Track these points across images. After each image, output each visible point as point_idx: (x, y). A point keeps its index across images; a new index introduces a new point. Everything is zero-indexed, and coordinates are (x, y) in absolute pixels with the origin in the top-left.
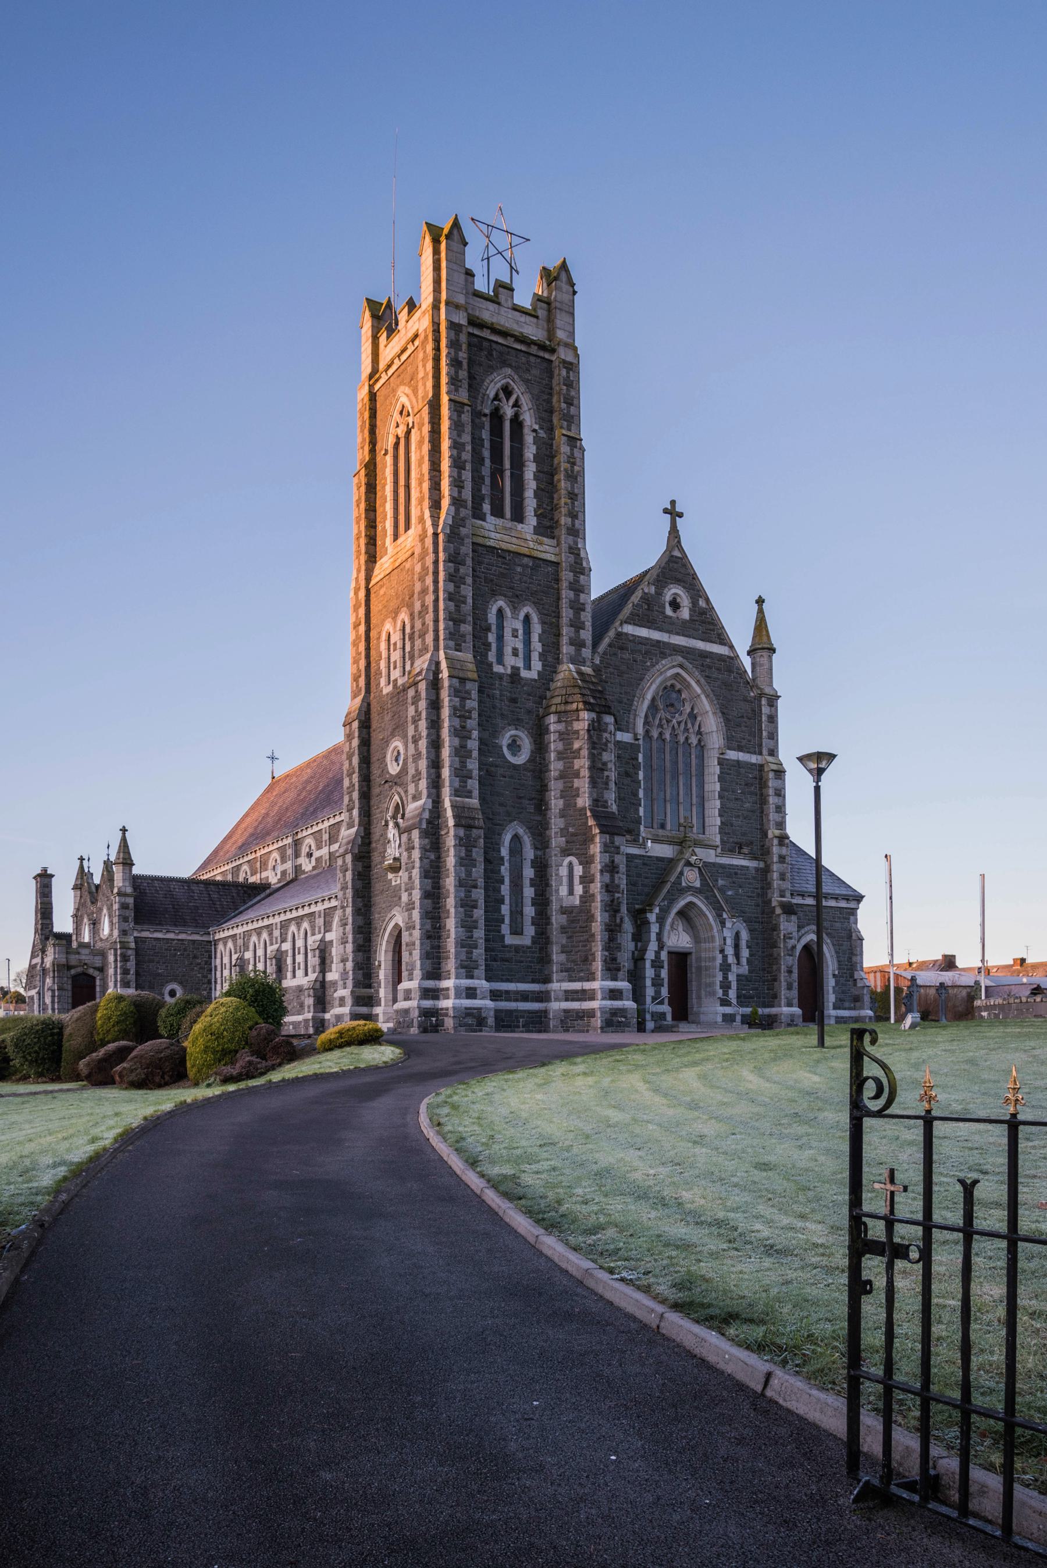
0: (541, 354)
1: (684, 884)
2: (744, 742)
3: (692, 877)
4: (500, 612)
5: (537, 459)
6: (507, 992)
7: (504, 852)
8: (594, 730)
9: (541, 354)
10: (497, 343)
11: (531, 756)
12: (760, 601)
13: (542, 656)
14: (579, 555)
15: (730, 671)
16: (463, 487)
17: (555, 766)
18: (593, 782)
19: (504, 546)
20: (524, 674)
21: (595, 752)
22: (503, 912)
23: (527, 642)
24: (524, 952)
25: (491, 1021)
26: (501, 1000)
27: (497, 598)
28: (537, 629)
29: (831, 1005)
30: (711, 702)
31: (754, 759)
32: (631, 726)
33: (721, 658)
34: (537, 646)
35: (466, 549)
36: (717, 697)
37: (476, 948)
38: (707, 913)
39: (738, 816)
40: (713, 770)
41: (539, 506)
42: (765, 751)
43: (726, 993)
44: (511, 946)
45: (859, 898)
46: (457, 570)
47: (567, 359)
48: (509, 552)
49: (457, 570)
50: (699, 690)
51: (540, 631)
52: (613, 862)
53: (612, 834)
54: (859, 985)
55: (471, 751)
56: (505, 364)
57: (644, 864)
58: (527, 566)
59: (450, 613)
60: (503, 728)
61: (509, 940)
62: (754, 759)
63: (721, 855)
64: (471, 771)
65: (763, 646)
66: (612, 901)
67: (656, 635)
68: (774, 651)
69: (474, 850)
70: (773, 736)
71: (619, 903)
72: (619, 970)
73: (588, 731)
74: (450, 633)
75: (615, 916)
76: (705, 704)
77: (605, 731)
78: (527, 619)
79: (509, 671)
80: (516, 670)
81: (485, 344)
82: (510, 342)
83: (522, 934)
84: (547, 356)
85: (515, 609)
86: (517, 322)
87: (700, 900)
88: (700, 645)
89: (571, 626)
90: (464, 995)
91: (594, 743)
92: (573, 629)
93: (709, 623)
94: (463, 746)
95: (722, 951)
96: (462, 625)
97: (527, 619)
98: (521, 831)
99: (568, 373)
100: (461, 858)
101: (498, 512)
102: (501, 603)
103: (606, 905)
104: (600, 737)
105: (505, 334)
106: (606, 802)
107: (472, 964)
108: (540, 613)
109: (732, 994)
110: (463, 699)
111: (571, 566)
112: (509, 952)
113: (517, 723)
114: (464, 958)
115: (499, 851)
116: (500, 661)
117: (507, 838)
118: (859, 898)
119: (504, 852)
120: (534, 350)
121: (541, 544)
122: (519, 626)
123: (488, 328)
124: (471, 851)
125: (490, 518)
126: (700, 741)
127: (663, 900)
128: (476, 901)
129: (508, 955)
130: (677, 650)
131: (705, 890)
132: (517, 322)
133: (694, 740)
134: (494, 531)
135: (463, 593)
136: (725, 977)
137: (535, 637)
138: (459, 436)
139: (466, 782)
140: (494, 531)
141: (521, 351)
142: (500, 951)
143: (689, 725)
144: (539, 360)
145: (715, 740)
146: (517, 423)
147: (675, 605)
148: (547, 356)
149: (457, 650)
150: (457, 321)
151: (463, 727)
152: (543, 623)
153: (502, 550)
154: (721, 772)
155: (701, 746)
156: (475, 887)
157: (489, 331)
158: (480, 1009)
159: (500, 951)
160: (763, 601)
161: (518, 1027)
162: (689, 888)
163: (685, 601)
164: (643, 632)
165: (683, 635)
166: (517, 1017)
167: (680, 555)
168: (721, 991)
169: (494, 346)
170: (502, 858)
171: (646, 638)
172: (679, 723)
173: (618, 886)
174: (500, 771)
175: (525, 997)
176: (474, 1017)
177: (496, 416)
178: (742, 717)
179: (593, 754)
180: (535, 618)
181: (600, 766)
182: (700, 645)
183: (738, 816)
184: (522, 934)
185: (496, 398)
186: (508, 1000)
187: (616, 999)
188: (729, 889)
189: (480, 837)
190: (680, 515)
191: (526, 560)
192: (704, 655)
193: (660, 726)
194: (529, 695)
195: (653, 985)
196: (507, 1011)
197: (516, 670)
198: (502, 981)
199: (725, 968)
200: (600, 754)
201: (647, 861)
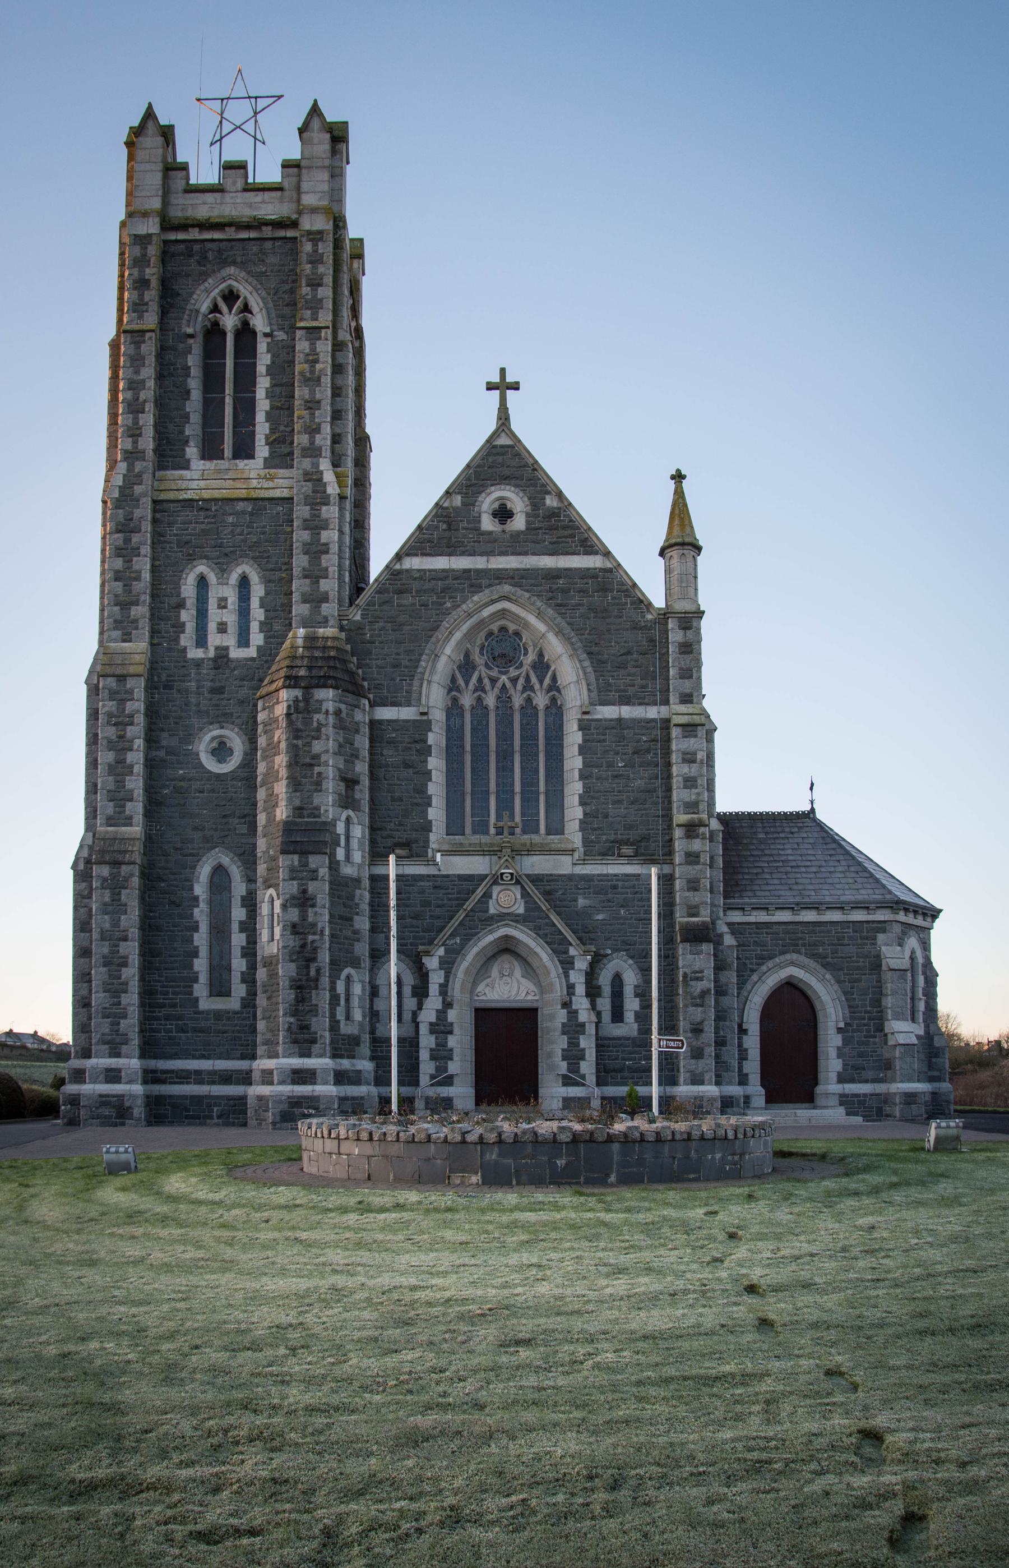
0: (282, 233)
1: (492, 911)
2: (631, 691)
3: (507, 899)
4: (202, 582)
5: (270, 371)
6: (198, 1072)
7: (200, 890)
8: (297, 711)
9: (282, 233)
10: (213, 240)
11: (244, 759)
12: (678, 477)
13: (265, 626)
14: (320, 480)
15: (604, 589)
16: (140, 435)
17: (427, 1041)
18: (295, 784)
19: (206, 494)
20: (236, 653)
21: (300, 742)
22: (196, 968)
23: (244, 613)
24: (229, 1019)
25: (139, 1111)
26: (188, 1083)
27: (195, 563)
28: (258, 591)
29: (833, 1076)
30: (566, 639)
31: (652, 712)
32: (414, 696)
33: (586, 574)
34: (257, 613)
35: (144, 511)
36: (579, 631)
37: (125, 1017)
38: (538, 950)
39: (619, 802)
40: (573, 737)
41: (273, 430)
42: (673, 698)
43: (573, 1067)
44: (208, 1012)
45: (932, 913)
46: (127, 541)
47: (315, 228)
48: (216, 500)
49: (127, 541)
50: (542, 627)
51: (262, 593)
52: (305, 891)
53: (304, 853)
54: (891, 1043)
55: (132, 766)
56: (225, 263)
57: (435, 887)
58: (244, 512)
59: (116, 596)
60: (201, 729)
61: (207, 1003)
62: (652, 712)
63: (583, 861)
64: (132, 791)
65: (681, 544)
66: (303, 946)
67: (479, 563)
68: (698, 549)
69: (123, 892)
70: (692, 671)
71: (315, 949)
72: (314, 1041)
73: (288, 715)
74: (115, 621)
75: (308, 967)
76: (555, 647)
77: (318, 711)
78: (244, 582)
79: (211, 654)
80: (222, 652)
81: (196, 247)
82: (231, 233)
83: (229, 995)
84: (290, 233)
85: (223, 571)
86: (250, 205)
87: (523, 932)
88: (548, 562)
89: (305, 577)
90: (102, 1077)
91: (298, 730)
92: (308, 581)
93: (565, 528)
94: (120, 761)
95: (566, 1005)
96: (133, 608)
97: (244, 582)
98: (226, 860)
99: (315, 246)
100: (105, 904)
101: (211, 451)
102: (202, 568)
103: (291, 954)
104: (308, 721)
105: (219, 226)
106: (318, 808)
107: (118, 1039)
108: (263, 569)
109: (588, 1067)
110: (122, 702)
111: (307, 497)
112: (206, 1019)
113: (222, 718)
114: (107, 1031)
115: (192, 889)
116: (201, 641)
117: (204, 871)
118: (932, 913)
119: (200, 890)
120: (267, 232)
121: (272, 479)
122: (231, 595)
123: (193, 226)
124: (119, 893)
125: (198, 465)
126: (554, 700)
127: (452, 935)
128: (127, 957)
129: (203, 1024)
130: (500, 576)
131: (532, 918)
132: (250, 205)
133: (541, 700)
134: (199, 478)
135: (136, 567)
136: (573, 1043)
137: (255, 603)
138: (137, 372)
139: (124, 806)
140: (199, 478)
141: (249, 239)
142: (191, 1019)
143: (534, 680)
144: (278, 243)
145: (575, 695)
146: (246, 333)
147: (503, 514)
148: (290, 233)
149: (124, 641)
150: (144, 232)
151: (121, 737)
152: (267, 581)
153: (204, 500)
154: (585, 741)
155: (556, 710)
156: (125, 939)
157: (197, 230)
158: (123, 1096)
159: (191, 1019)
160: (684, 477)
161: (211, 1118)
162: (502, 917)
163: (518, 503)
164: (440, 563)
165: (513, 554)
166: (209, 1105)
167: (509, 442)
168: (564, 1065)
169: (209, 245)
170: (196, 899)
171: (443, 571)
172: (514, 681)
173: (314, 925)
174: (196, 785)
175: (226, 1078)
176: (114, 1107)
177: (214, 332)
178: (629, 653)
179: (296, 746)
180: (254, 578)
181: (308, 760)
182: (548, 562)
183: (619, 802)
184: (229, 995)
185: (215, 309)
186: (201, 1082)
187: (304, 1083)
188: (599, 912)
189: (132, 875)
190: (515, 386)
191: (240, 506)
192: (553, 575)
193: (480, 687)
194: (242, 680)
195: (433, 1058)
196: (192, 1097)
197: (222, 652)
198: (194, 1057)
199: (573, 1029)
200: (309, 744)
201: (440, 882)
